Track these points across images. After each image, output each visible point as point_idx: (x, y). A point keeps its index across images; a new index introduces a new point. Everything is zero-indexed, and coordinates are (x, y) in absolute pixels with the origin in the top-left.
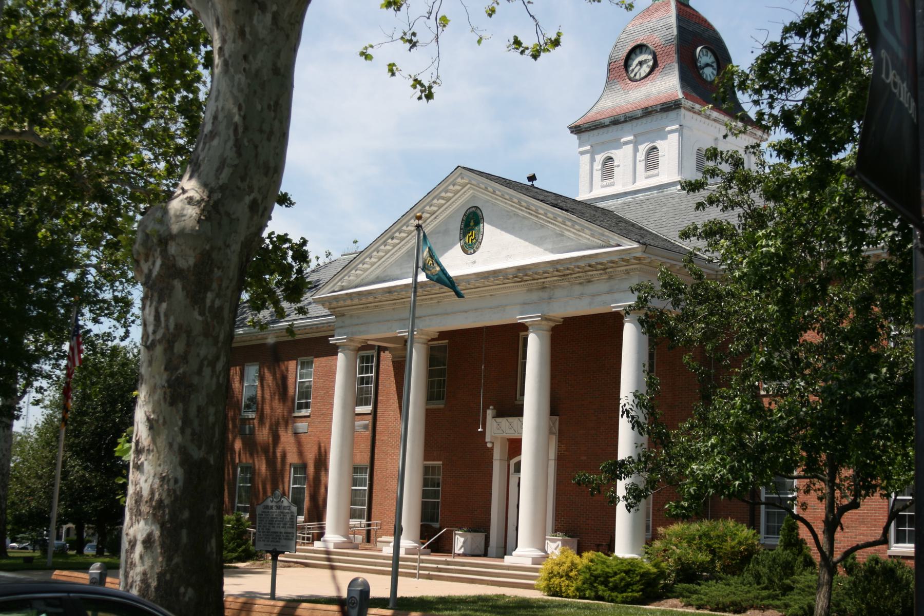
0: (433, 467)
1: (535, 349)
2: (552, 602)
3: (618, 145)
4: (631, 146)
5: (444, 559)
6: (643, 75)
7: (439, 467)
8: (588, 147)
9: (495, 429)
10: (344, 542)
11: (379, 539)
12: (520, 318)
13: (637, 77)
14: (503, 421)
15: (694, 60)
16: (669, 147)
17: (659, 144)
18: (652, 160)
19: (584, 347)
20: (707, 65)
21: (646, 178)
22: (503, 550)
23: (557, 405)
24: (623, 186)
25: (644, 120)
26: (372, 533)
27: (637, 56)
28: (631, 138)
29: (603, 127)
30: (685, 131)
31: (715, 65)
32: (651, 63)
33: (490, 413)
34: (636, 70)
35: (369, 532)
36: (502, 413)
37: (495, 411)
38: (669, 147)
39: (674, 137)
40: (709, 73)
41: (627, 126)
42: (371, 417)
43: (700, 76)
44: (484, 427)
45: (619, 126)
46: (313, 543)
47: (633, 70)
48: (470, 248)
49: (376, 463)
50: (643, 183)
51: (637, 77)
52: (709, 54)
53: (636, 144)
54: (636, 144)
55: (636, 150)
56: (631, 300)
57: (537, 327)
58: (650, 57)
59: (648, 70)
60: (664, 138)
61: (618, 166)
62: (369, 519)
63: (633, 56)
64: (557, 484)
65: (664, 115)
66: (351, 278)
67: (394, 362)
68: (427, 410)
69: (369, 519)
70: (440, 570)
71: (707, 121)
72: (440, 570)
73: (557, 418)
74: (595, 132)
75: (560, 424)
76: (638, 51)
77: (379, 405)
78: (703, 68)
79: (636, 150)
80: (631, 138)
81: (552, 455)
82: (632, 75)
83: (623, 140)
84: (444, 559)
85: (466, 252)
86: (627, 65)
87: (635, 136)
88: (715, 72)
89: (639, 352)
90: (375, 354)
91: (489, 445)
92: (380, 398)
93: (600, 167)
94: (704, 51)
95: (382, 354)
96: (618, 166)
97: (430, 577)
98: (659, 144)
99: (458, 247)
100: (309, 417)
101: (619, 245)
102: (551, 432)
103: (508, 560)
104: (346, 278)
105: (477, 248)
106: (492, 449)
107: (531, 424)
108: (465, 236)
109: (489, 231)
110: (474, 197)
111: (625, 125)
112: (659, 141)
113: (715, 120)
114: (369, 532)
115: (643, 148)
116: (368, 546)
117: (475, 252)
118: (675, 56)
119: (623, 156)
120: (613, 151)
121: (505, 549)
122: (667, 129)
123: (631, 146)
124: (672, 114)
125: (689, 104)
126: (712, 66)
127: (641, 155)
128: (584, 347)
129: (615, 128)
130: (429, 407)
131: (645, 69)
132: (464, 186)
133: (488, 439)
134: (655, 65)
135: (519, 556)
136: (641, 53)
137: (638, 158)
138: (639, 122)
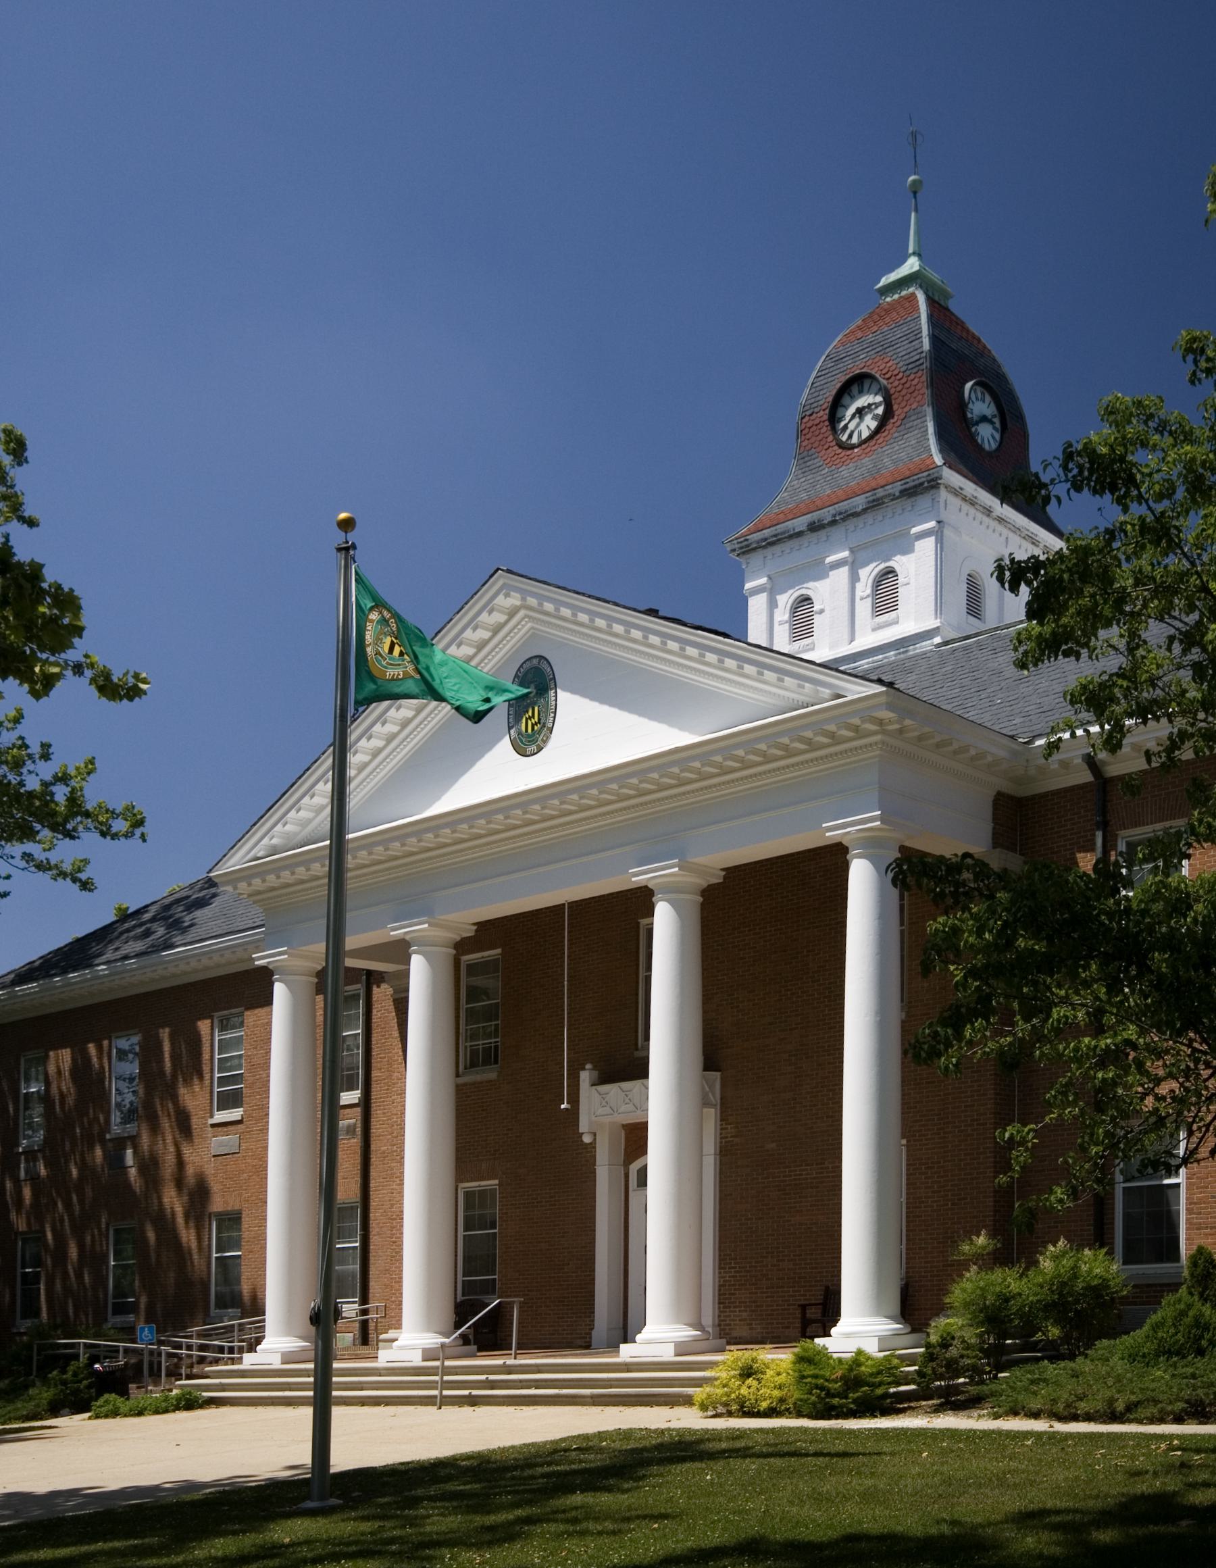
0: (482, 1193)
1: (666, 927)
2: (716, 1435)
3: (819, 571)
4: (844, 572)
5: (500, 1362)
6: (865, 434)
7: (493, 1191)
8: (764, 580)
9: (597, 1108)
10: (696, 1340)
11: (382, 1337)
12: (639, 876)
13: (855, 440)
14: (613, 1090)
15: (962, 406)
16: (917, 568)
17: (900, 563)
18: (885, 594)
19: (769, 925)
20: (984, 419)
21: (874, 630)
22: (621, 1332)
23: (715, 1051)
24: (831, 648)
25: (869, 517)
26: (372, 1325)
27: (853, 398)
28: (845, 554)
29: (791, 537)
30: (947, 532)
31: (997, 421)
32: (880, 411)
33: (585, 1076)
34: (851, 426)
35: (364, 1325)
36: (609, 1075)
37: (596, 1073)
38: (917, 568)
39: (926, 547)
40: (987, 435)
41: (837, 533)
42: (359, 1110)
43: (972, 438)
44: (574, 1100)
45: (823, 533)
46: (240, 1360)
47: (846, 427)
48: (529, 743)
49: (373, 1195)
50: (867, 639)
51: (855, 440)
52: (988, 398)
53: (854, 566)
54: (854, 566)
55: (854, 578)
56: (869, 819)
57: (672, 890)
58: (879, 399)
59: (873, 425)
60: (907, 550)
61: (821, 612)
62: (364, 1300)
63: (840, 411)
64: (720, 1219)
65: (908, 503)
66: (288, 827)
67: (394, 1000)
68: (457, 1086)
69: (364, 1300)
70: (493, 1385)
71: (986, 520)
72: (493, 1385)
73: (718, 1074)
74: (777, 549)
75: (723, 1086)
76: (855, 389)
77: (375, 1087)
78: (977, 423)
79: (854, 578)
80: (845, 554)
81: (710, 1147)
82: (844, 438)
83: (828, 560)
84: (500, 1362)
85: (524, 754)
86: (834, 418)
87: (852, 550)
88: (997, 436)
89: (882, 916)
90: (362, 993)
91: (587, 1139)
92: (375, 1074)
93: (786, 617)
94: (979, 389)
95: (375, 989)
96: (821, 612)
97: (473, 1401)
98: (900, 563)
99: (506, 742)
100: (240, 1122)
101: (839, 696)
102: (706, 1103)
103: (627, 1352)
104: (279, 827)
105: (545, 742)
106: (593, 1145)
107: (664, 1091)
108: (518, 720)
109: (569, 705)
110: (533, 637)
111: (833, 529)
112: (898, 558)
113: (1000, 520)
114: (364, 1325)
115: (868, 574)
116: (364, 1350)
117: (540, 749)
118: (927, 392)
119: (829, 591)
120: (811, 584)
121: (626, 1332)
122: (914, 530)
123: (844, 572)
124: (923, 501)
125: (952, 478)
126: (992, 423)
127: (864, 587)
128: (769, 925)
129: (813, 537)
130: (461, 1080)
131: (869, 423)
132: (512, 613)
133: (583, 1127)
134: (883, 422)
135: (649, 1342)
136: (861, 392)
137: (859, 594)
138: (859, 521)
